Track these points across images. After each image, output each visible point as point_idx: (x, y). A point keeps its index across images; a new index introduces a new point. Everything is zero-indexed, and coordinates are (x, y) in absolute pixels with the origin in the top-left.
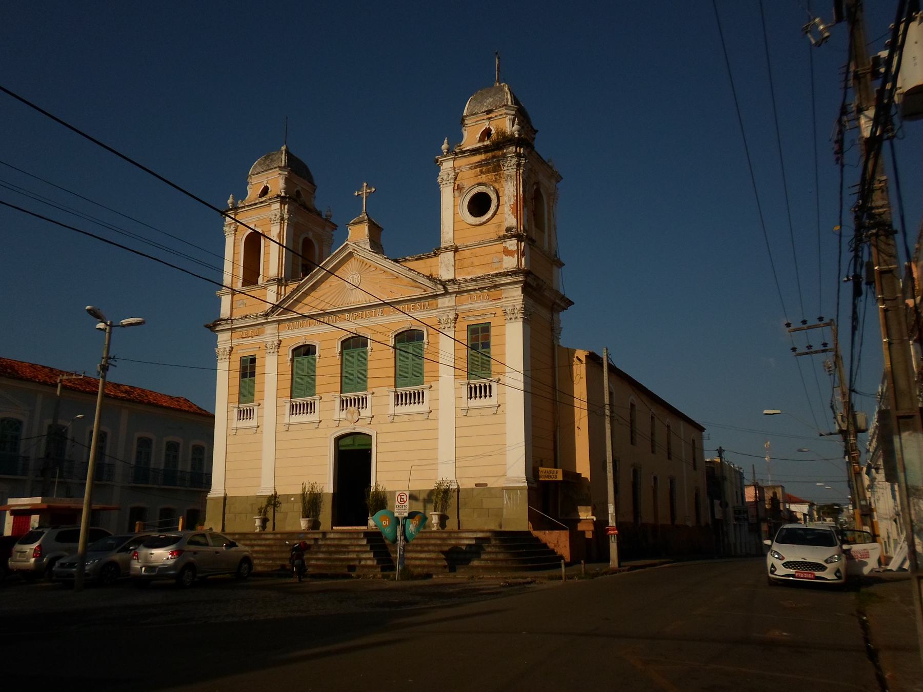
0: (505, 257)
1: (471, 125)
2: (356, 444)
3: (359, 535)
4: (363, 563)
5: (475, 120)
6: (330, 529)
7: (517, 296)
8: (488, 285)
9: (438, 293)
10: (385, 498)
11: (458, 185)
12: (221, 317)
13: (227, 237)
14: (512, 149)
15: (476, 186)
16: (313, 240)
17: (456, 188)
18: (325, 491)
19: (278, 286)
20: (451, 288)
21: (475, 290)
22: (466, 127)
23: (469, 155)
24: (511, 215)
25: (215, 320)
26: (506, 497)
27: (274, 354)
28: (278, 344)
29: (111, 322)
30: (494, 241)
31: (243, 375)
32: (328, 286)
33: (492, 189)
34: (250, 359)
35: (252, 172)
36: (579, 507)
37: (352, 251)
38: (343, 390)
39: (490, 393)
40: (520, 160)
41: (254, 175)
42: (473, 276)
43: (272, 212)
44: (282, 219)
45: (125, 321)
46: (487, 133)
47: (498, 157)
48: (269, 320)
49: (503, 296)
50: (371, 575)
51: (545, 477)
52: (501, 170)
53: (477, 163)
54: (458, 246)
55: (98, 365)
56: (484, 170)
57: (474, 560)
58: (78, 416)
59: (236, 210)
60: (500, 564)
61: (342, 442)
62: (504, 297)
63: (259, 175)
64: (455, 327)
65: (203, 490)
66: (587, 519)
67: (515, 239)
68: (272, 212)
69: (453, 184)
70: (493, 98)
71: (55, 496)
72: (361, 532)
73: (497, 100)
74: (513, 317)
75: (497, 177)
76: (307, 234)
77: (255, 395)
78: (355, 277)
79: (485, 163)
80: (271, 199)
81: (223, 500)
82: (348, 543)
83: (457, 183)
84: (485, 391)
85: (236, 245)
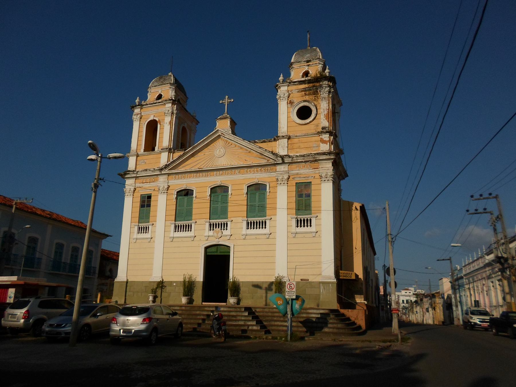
0: (321, 144)
1: (296, 68)
2: (219, 251)
3: (241, 309)
4: (250, 328)
5: (299, 65)
6: (201, 304)
7: (329, 167)
8: (311, 160)
9: (278, 162)
10: (239, 285)
11: (290, 101)
12: (129, 169)
13: (134, 121)
14: (326, 82)
15: (303, 102)
16: (187, 129)
17: (289, 102)
18: (197, 280)
19: (169, 153)
20: (287, 160)
21: (302, 162)
22: (293, 69)
23: (298, 84)
24: (325, 120)
25: (125, 171)
26: (322, 287)
27: (164, 194)
28: (167, 188)
29: (102, 155)
30: (315, 134)
31: (142, 206)
32: (203, 154)
33: (313, 104)
34: (148, 196)
35: (151, 85)
36: (355, 295)
37: (220, 134)
38: (211, 218)
39: (311, 224)
40: (331, 89)
41: (153, 87)
42: (302, 154)
43: (166, 109)
44: (172, 113)
45: (112, 155)
46: (306, 74)
47: (317, 86)
48: (162, 173)
49: (320, 167)
50: (264, 337)
51: (344, 276)
52: (318, 94)
53: (303, 89)
54: (291, 135)
55: (93, 184)
56: (307, 93)
57: (325, 328)
58: (27, 226)
59: (141, 106)
60: (341, 331)
61: (208, 250)
62: (321, 167)
63: (156, 87)
64: (288, 184)
65: (91, 276)
66: (361, 303)
67: (328, 134)
68: (166, 109)
69: (287, 100)
70: (310, 54)
71: (21, 275)
72: (243, 307)
73: (313, 55)
74: (326, 179)
75: (316, 98)
76: (184, 124)
77: (150, 218)
78: (221, 150)
79: (309, 89)
80: (166, 101)
81: (126, 283)
82: (235, 314)
83: (289, 99)
84: (307, 223)
85: (140, 127)
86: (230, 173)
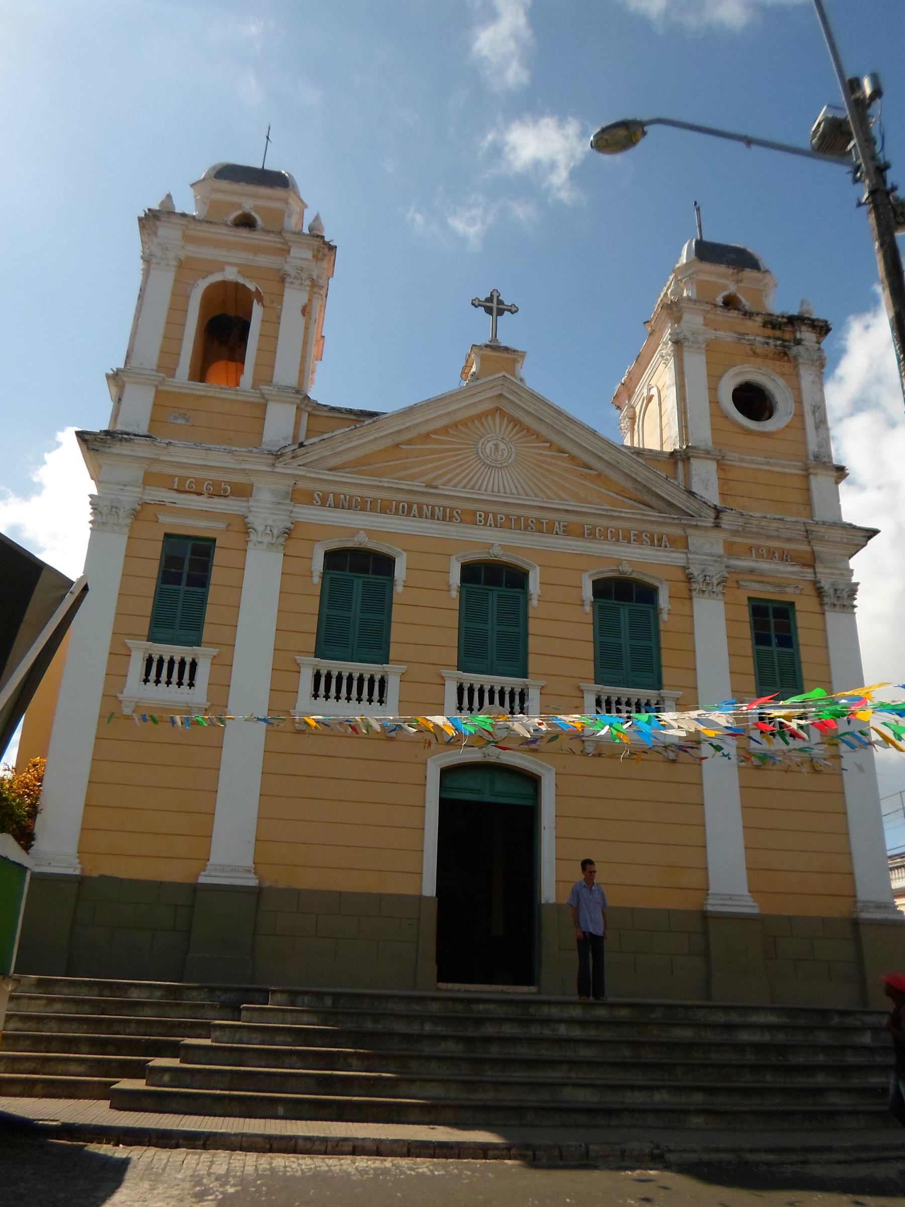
48: (276, 470)
78: (502, 446)
86: (458, 517)
